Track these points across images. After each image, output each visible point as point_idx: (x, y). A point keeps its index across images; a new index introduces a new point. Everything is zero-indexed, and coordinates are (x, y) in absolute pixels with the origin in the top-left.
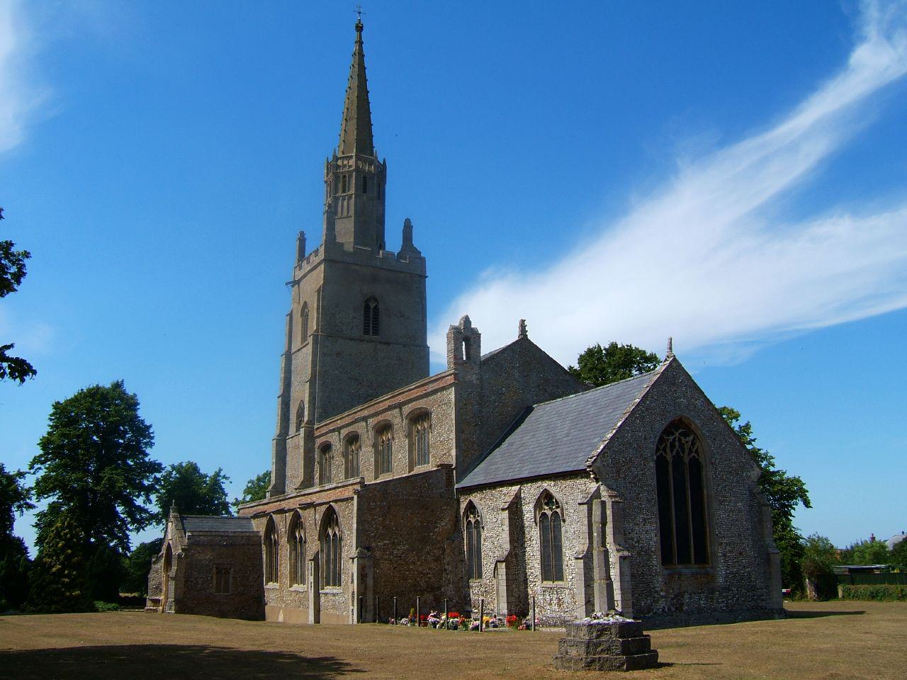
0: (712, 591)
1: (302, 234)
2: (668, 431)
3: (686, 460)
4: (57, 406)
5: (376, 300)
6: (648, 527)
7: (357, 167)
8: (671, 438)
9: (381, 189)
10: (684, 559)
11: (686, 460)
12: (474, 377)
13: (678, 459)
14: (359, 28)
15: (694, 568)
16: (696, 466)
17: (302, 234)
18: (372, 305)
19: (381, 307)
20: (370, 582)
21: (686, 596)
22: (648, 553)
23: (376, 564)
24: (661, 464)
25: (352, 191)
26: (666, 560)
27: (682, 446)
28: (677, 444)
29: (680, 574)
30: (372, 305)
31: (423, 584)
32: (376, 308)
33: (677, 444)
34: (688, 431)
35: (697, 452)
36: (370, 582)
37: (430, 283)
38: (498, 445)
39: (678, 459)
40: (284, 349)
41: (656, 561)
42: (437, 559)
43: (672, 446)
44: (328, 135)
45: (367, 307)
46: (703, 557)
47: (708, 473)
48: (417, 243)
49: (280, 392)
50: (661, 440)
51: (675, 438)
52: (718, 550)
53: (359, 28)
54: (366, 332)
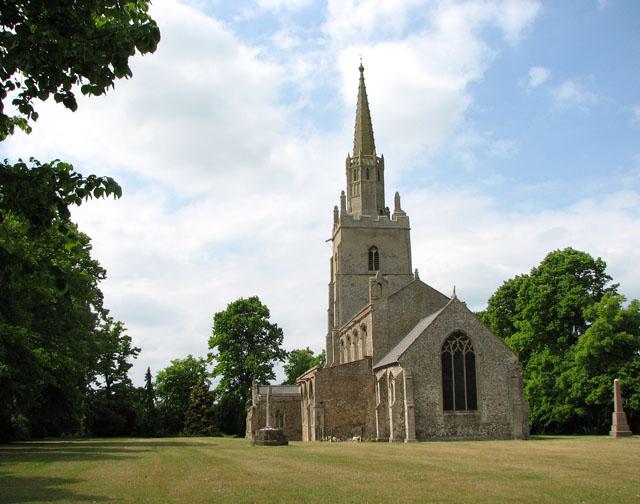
0: (478, 425)
1: (397, 194)
3: (464, 353)
4: (218, 316)
5: (376, 248)
6: (434, 390)
7: (362, 162)
10: (460, 407)
11: (464, 353)
13: (458, 354)
14: (362, 69)
15: (467, 412)
16: (471, 357)
17: (397, 194)
18: (374, 251)
19: (380, 252)
20: (322, 419)
21: (460, 427)
23: (326, 411)
24: (445, 358)
25: (360, 180)
26: (447, 406)
27: (461, 346)
29: (455, 416)
30: (374, 251)
31: (355, 422)
32: (377, 253)
35: (472, 348)
36: (322, 419)
37: (412, 234)
38: (416, 339)
39: (458, 354)
40: (329, 281)
41: (439, 409)
42: (363, 408)
43: (455, 346)
44: (345, 145)
45: (370, 253)
46: (473, 406)
49: (328, 308)
50: (446, 343)
53: (362, 69)
54: (371, 269)
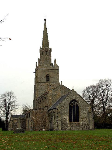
2: (72, 101)
5: (49, 75)
8: (73, 102)
9: (50, 53)
10: (74, 121)
12: (52, 92)
13: (74, 106)
16: (78, 107)
22: (67, 120)
24: (70, 107)
26: (71, 121)
28: (74, 103)
33: (74, 103)
34: (76, 101)
35: (78, 104)
39: (74, 106)
41: (68, 121)
43: (73, 104)
45: (47, 76)
46: (78, 120)
47: (80, 108)
48: (57, 63)
50: (70, 103)
51: (73, 103)
52: (81, 120)
53: (45, 20)
